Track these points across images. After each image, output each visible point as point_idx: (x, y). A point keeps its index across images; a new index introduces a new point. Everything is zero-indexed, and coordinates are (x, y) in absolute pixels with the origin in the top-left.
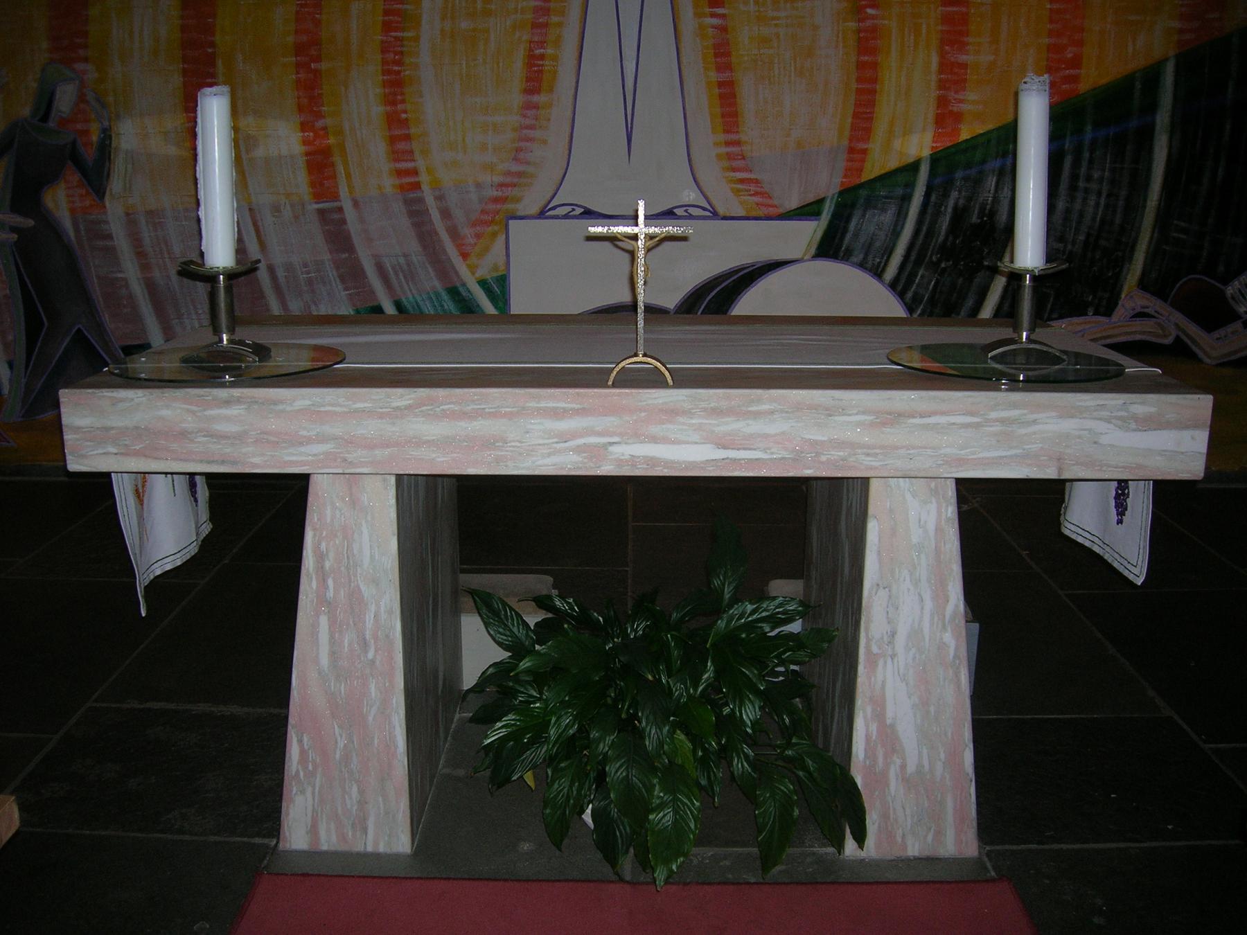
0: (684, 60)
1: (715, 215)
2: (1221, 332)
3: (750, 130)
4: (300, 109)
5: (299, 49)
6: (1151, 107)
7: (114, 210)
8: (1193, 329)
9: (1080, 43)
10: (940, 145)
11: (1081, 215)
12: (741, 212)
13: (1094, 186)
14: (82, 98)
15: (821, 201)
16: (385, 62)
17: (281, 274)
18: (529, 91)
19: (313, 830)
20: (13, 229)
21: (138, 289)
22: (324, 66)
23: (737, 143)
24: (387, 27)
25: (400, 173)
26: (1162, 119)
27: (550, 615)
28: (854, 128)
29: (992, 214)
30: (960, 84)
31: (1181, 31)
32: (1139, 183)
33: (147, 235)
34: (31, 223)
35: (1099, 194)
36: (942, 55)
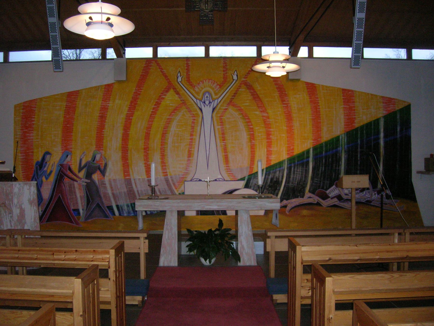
0: (218, 149)
1: (224, 180)
2: (326, 200)
3: (231, 164)
4: (145, 160)
5: (145, 149)
6: (308, 157)
7: (106, 179)
8: (321, 200)
9: (293, 146)
10: (267, 166)
11: (296, 178)
12: (229, 180)
13: (298, 173)
14: (101, 157)
15: (245, 177)
16: (161, 152)
17: (140, 192)
18: (188, 157)
19: (164, 263)
20: (86, 182)
21: (110, 195)
22: (149, 152)
23: (228, 166)
24: (162, 145)
25: (164, 173)
26: (311, 159)
27: (191, 242)
28: (251, 163)
29: (278, 179)
30: (271, 154)
31: (313, 143)
32: (307, 171)
33: (113, 184)
34: (89, 181)
35: (299, 174)
36: (267, 148)
